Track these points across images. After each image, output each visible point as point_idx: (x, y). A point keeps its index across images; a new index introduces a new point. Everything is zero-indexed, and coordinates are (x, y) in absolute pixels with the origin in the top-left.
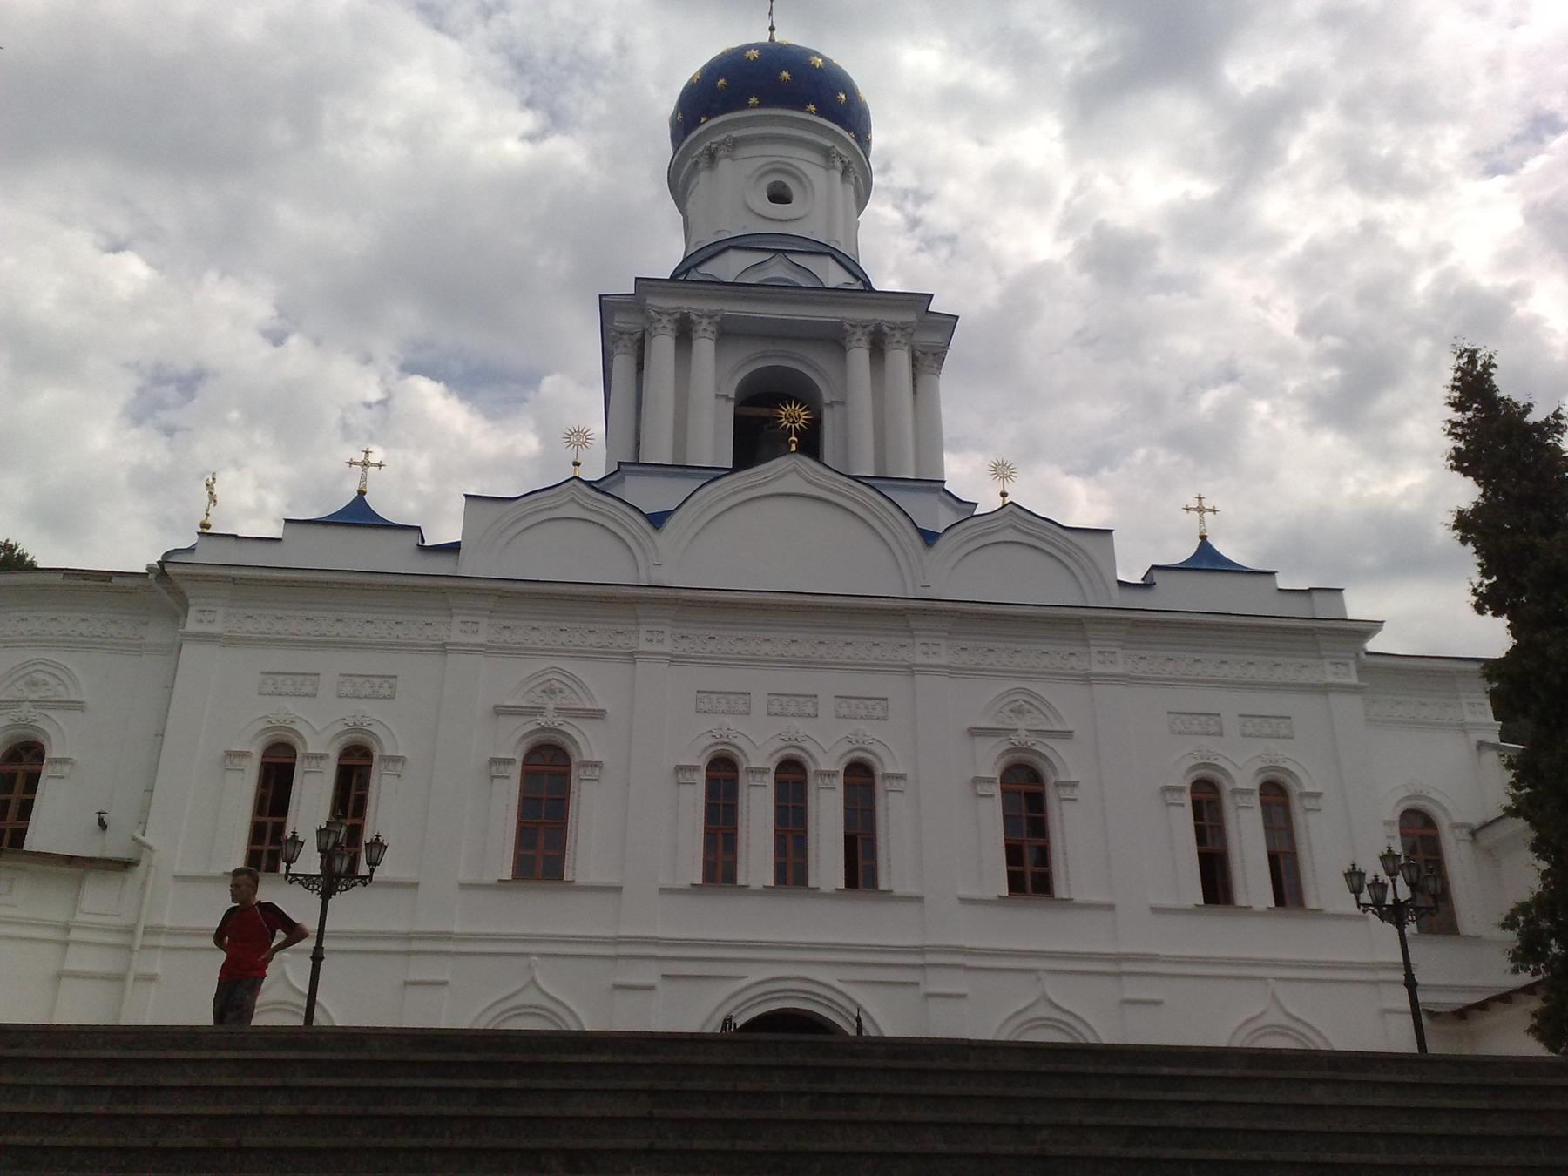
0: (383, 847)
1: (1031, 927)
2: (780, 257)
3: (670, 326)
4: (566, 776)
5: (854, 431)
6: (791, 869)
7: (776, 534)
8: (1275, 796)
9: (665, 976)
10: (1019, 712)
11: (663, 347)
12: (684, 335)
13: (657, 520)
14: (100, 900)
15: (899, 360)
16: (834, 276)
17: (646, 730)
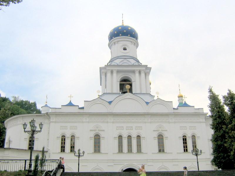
1: (161, 156)
2: (125, 60)
3: (110, 72)
4: (100, 139)
6: (130, 151)
7: (127, 104)
8: (193, 137)
9: (114, 164)
10: (160, 128)
11: (109, 75)
12: (112, 72)
13: (110, 103)
15: (143, 75)
16: (133, 62)
17: (110, 132)
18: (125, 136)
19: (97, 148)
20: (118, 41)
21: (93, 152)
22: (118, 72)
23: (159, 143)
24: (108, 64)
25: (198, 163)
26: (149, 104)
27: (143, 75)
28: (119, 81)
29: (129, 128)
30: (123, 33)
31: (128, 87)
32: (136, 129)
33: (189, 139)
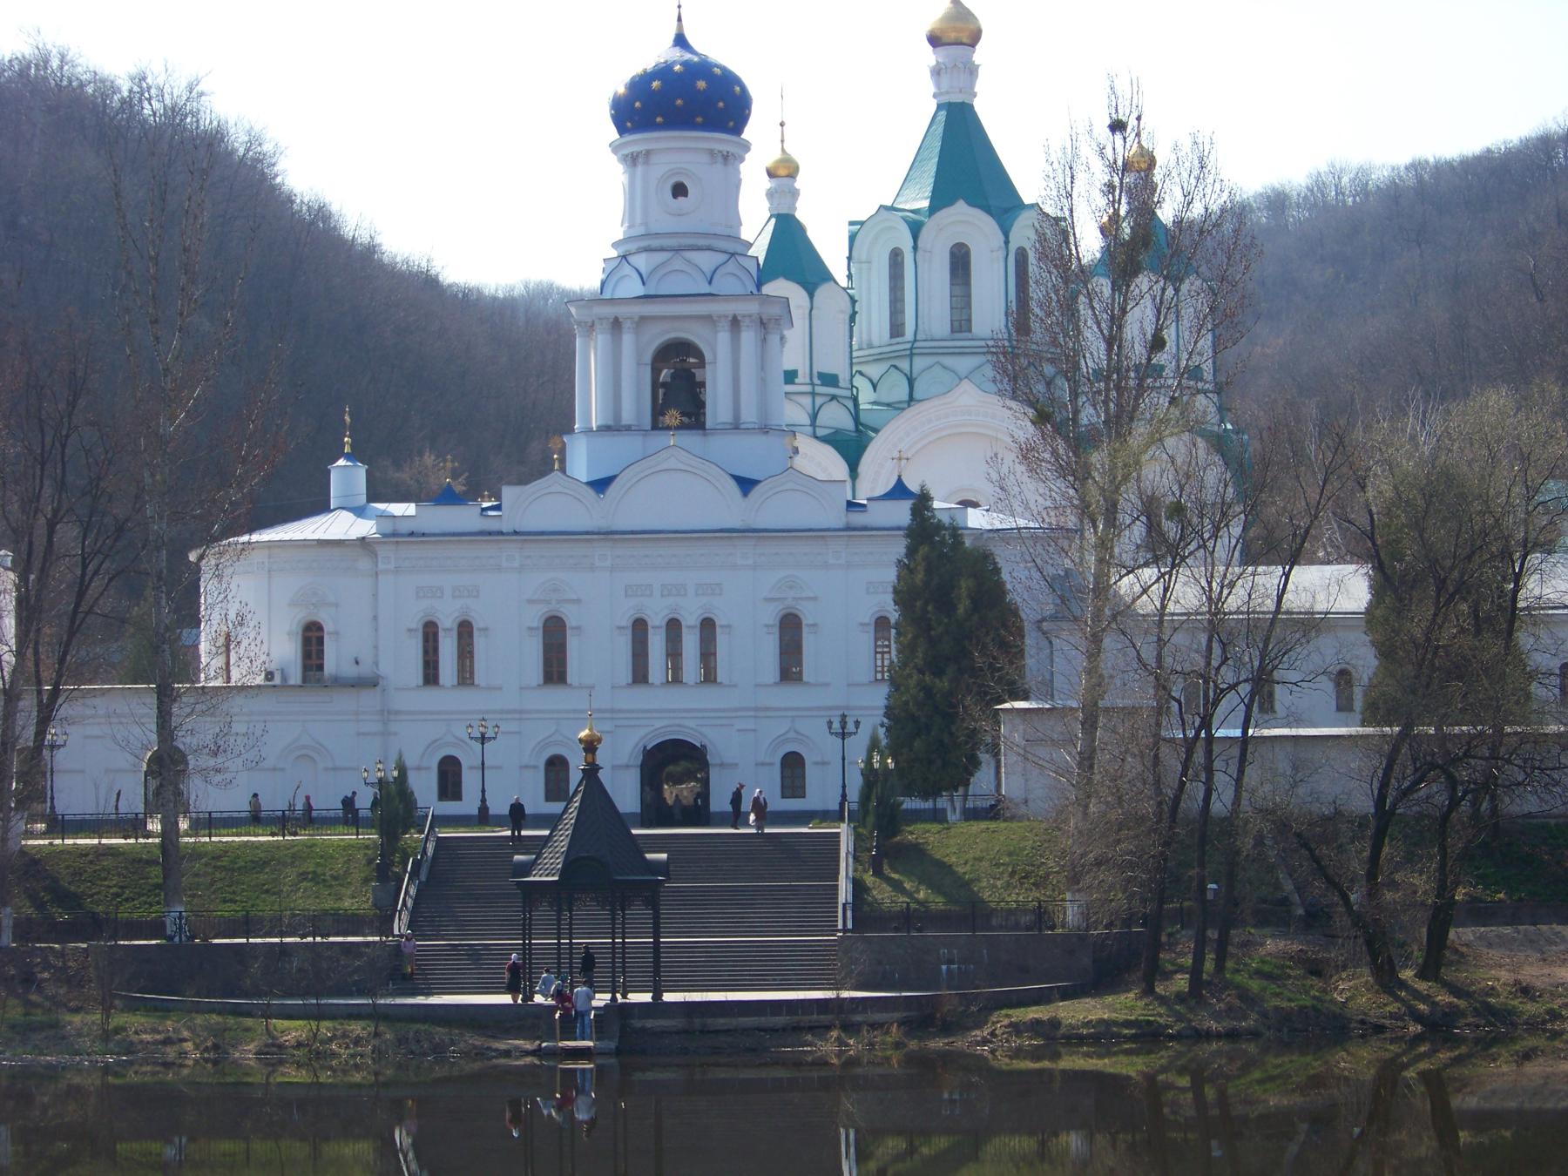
8: (708, 625)
10: (791, 587)
14: (368, 698)
15: (748, 337)
18: (657, 623)
20: (648, 153)
26: (756, 492)
27: (748, 337)
29: (673, 589)
32: (454, 597)
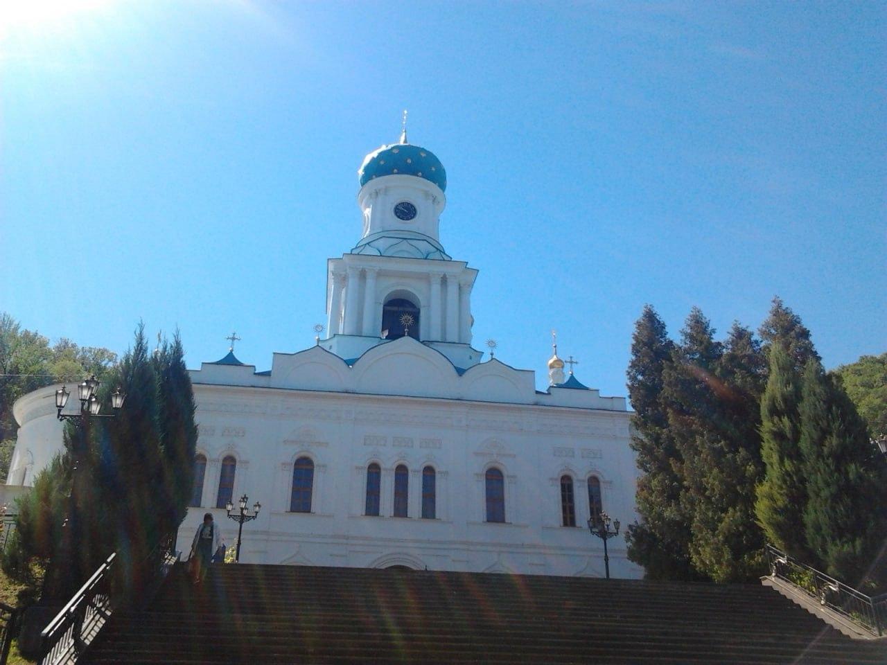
0: (247, 498)
2: (405, 241)
5: (430, 323)
6: (401, 510)
15: (452, 290)
19: (301, 500)
21: (392, 514)
22: (380, 274)
23: (369, 483)
24: (355, 252)
25: (606, 559)
26: (466, 375)
28: (382, 302)
29: (404, 441)
30: (410, 163)
31: (406, 319)
33: (579, 487)
